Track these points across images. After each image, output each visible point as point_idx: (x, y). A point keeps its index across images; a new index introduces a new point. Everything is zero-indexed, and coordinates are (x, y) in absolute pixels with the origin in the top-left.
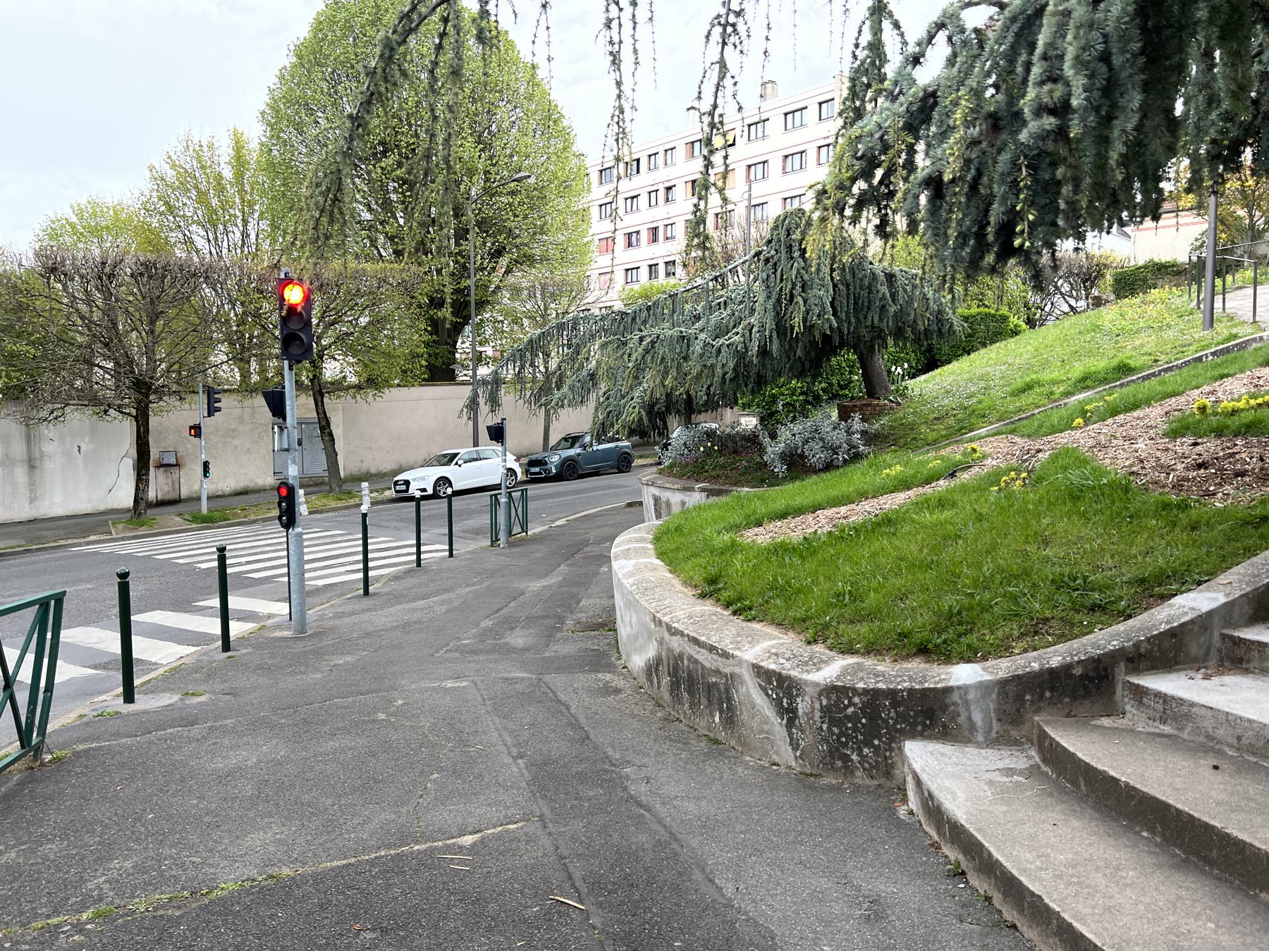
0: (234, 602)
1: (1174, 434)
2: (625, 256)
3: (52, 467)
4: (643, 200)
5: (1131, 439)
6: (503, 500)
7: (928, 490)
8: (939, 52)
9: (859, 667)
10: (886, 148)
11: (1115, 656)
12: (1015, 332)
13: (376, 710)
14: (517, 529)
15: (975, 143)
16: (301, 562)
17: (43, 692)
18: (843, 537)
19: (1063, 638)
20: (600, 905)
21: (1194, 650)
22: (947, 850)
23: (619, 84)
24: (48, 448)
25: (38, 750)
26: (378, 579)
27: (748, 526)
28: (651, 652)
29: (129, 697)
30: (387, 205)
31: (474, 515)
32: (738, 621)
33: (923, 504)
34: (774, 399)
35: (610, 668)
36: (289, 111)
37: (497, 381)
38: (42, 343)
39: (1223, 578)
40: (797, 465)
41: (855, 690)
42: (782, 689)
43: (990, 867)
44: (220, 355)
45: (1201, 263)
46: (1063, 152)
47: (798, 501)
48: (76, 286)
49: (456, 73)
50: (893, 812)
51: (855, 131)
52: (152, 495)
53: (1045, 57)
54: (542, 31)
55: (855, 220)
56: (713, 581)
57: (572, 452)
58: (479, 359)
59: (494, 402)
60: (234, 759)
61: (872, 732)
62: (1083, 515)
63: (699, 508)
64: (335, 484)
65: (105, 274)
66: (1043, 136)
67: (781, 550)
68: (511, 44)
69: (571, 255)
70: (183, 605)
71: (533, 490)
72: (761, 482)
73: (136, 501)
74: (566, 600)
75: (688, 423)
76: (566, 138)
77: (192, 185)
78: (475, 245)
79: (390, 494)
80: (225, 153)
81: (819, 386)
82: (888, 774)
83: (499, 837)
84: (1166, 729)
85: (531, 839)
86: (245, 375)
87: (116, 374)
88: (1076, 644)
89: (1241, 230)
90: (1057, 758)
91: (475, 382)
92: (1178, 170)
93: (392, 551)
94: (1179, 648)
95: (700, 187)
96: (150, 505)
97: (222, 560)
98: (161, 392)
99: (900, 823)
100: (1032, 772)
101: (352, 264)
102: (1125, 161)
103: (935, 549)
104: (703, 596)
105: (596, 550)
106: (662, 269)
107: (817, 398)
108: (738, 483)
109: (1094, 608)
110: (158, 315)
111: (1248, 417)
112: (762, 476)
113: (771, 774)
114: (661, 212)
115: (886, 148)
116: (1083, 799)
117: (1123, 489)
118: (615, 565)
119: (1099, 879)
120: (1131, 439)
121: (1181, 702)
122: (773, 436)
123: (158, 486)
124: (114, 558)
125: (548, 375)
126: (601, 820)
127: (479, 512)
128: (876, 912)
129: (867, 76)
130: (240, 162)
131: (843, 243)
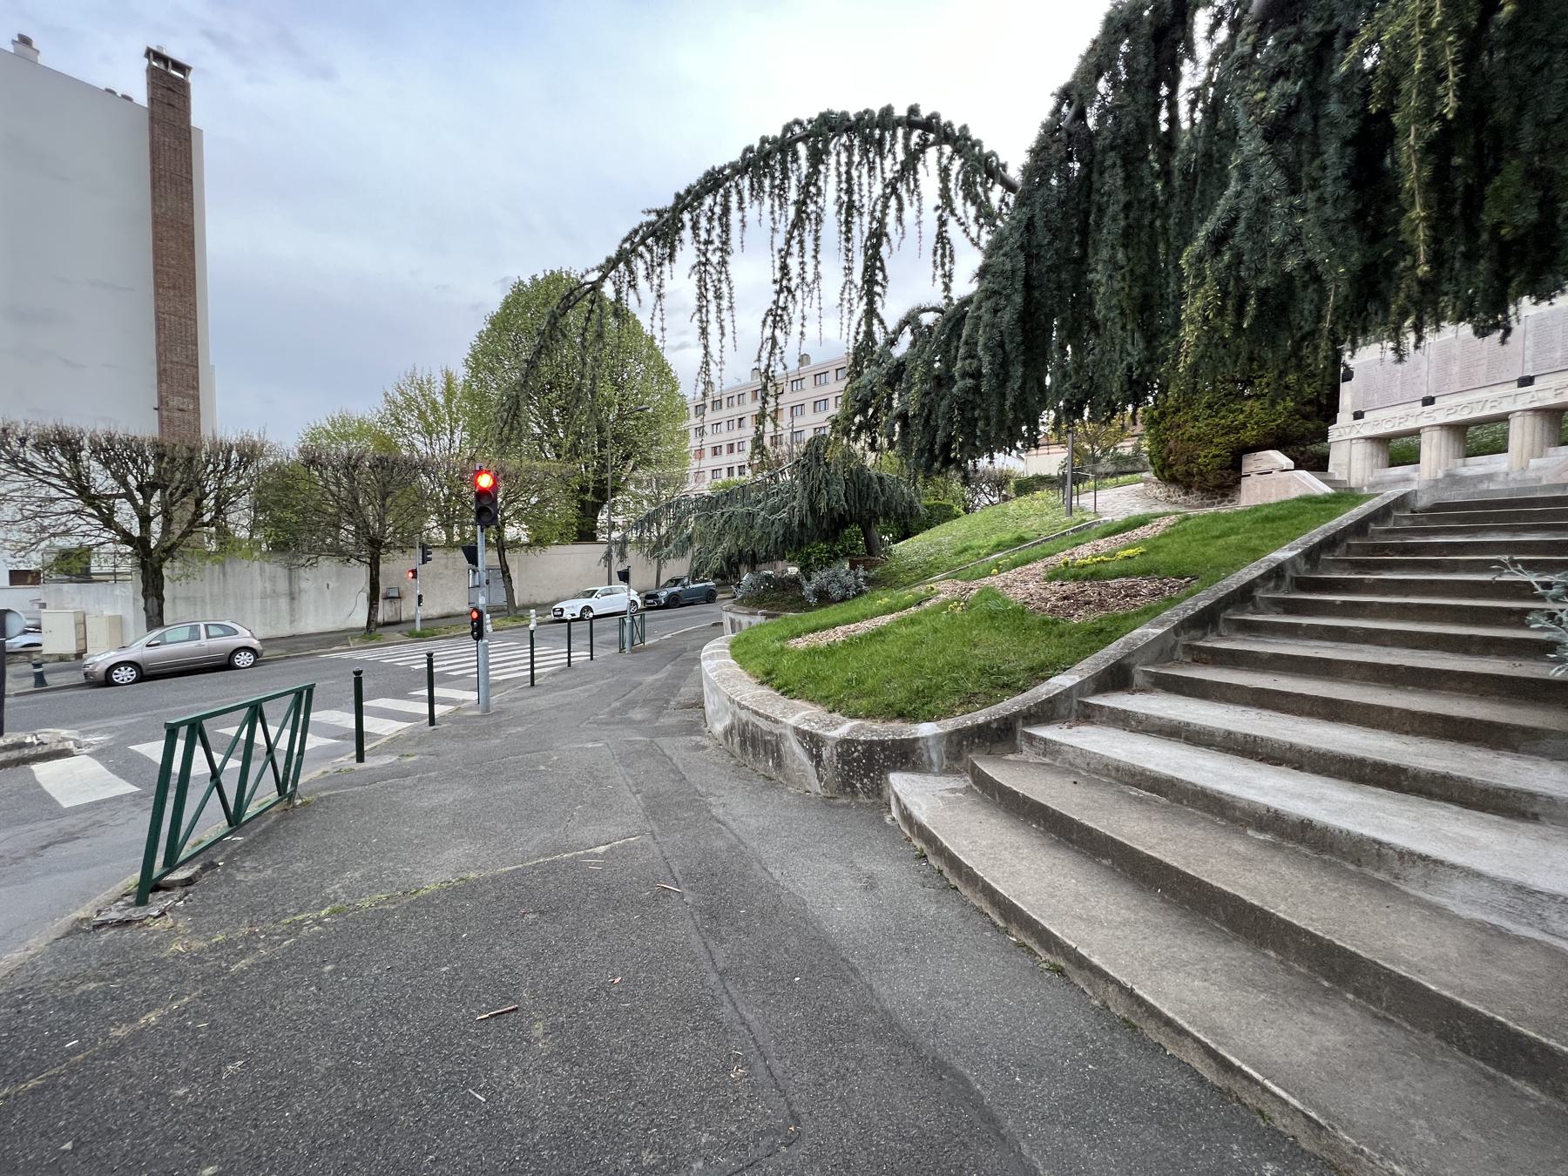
0: (437, 692)
1: (1050, 579)
2: (709, 462)
3: (308, 599)
4: (724, 425)
5: (1025, 582)
6: (628, 621)
7: (904, 613)
8: (906, 338)
9: (862, 727)
10: (874, 395)
11: (1016, 716)
12: (957, 516)
13: (538, 763)
14: (637, 641)
15: (927, 394)
16: (487, 664)
17: (296, 758)
18: (852, 643)
19: (985, 705)
20: (691, 889)
21: (1063, 711)
22: (916, 842)
23: (706, 347)
24: (304, 585)
25: (291, 797)
26: (541, 675)
27: (792, 637)
28: (727, 721)
29: (360, 757)
30: (551, 423)
31: (608, 632)
32: (785, 699)
33: (901, 622)
34: (809, 555)
35: (700, 732)
36: (484, 357)
37: (625, 541)
38: (303, 512)
39: (1078, 666)
40: (824, 598)
41: (859, 742)
42: (812, 742)
43: (941, 851)
44: (432, 522)
45: (1064, 476)
46: (979, 401)
47: (824, 621)
48: (329, 473)
49: (600, 336)
50: (883, 819)
51: (856, 384)
52: (380, 618)
53: (966, 343)
54: (658, 312)
55: (856, 440)
56: (768, 674)
57: (676, 589)
58: (613, 526)
59: (623, 555)
60: (436, 800)
61: (869, 768)
62: (997, 629)
63: (760, 626)
64: (511, 611)
65: (350, 466)
66: (966, 391)
67: (812, 652)
68: (637, 323)
69: (678, 458)
70: (401, 694)
71: (649, 615)
72: (801, 609)
73: (369, 622)
74: (671, 688)
75: (753, 569)
76: (674, 383)
77: (416, 405)
78: (613, 453)
79: (551, 617)
80: (439, 385)
81: (838, 548)
82: (879, 795)
83: (623, 846)
84: (1047, 760)
85: (644, 847)
86: (450, 536)
87: (357, 535)
88: (993, 708)
89: (1087, 457)
90: (982, 781)
91: (610, 542)
92: (1048, 416)
93: (551, 657)
94: (1053, 710)
95: (760, 418)
96: (379, 625)
97: (430, 662)
98: (388, 547)
99: (886, 826)
100: (968, 790)
101: (527, 462)
102: (1014, 408)
103: (909, 650)
104: (762, 683)
105: (691, 655)
106: (736, 471)
107: (836, 555)
108: (785, 610)
109: (1005, 686)
110: (388, 494)
111: (1093, 568)
112: (801, 605)
113: (805, 798)
114: (736, 434)
115: (874, 395)
116: (998, 806)
117: (1021, 612)
118: (704, 664)
119: (1006, 855)
120: (1025, 582)
121: (1055, 743)
122: (809, 579)
123: (384, 612)
124: (351, 661)
125: (659, 537)
126: (691, 832)
127: (612, 630)
128: (871, 884)
129: (864, 351)
130: (449, 392)
131: (849, 456)
